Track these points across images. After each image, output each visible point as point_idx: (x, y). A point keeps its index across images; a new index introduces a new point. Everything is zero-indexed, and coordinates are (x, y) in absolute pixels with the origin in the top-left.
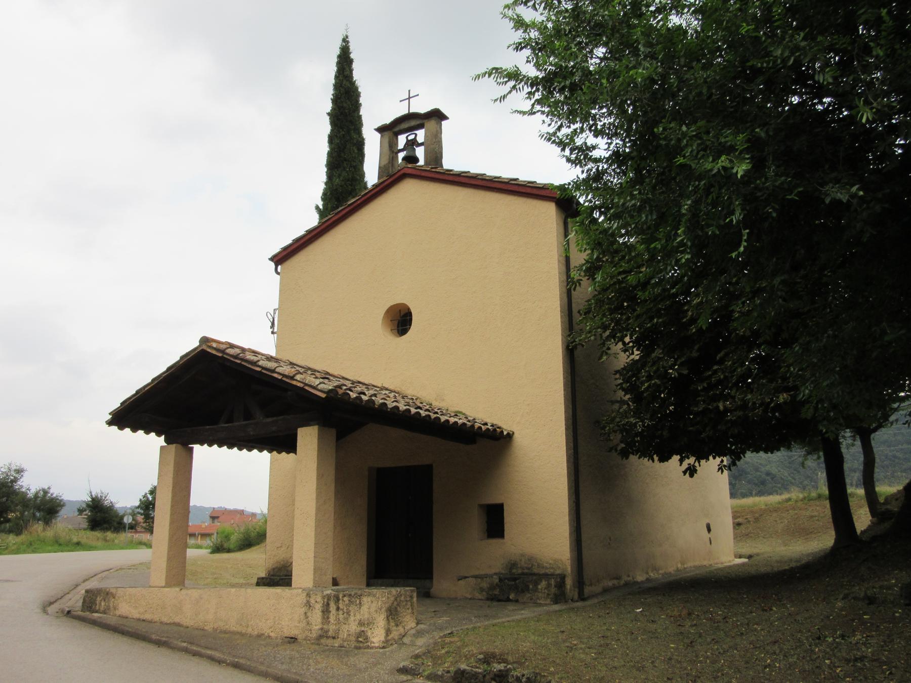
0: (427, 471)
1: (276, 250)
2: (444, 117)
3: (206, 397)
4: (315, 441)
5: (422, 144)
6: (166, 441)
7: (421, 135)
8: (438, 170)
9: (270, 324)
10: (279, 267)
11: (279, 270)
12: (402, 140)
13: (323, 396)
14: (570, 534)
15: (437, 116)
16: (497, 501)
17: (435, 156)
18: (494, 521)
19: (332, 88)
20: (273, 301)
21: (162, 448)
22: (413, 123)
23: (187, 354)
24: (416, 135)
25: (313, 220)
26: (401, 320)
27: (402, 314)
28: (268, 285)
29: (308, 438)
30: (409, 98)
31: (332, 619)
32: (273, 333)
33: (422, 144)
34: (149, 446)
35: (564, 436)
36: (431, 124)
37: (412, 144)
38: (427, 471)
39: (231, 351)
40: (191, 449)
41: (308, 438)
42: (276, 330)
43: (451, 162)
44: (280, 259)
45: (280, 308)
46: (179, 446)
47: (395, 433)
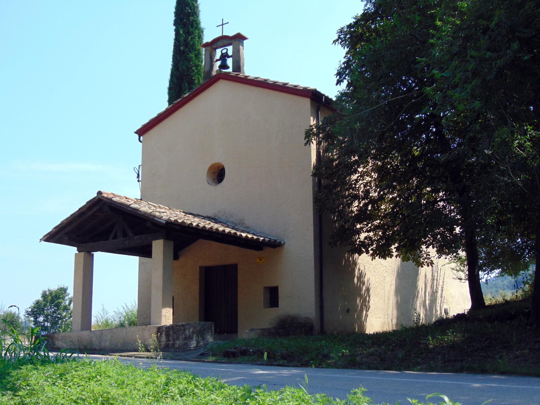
0: (234, 268)
1: (139, 127)
2: (245, 38)
3: (99, 226)
4: (162, 248)
5: (231, 56)
6: (78, 250)
7: (230, 50)
8: (241, 75)
9: (137, 175)
10: (141, 138)
11: (141, 139)
12: (218, 53)
13: (164, 222)
14: (316, 303)
15: (239, 38)
16: (275, 285)
17: (238, 67)
18: (273, 296)
19: (173, 15)
20: (138, 161)
21: (76, 254)
22: (225, 42)
23: (90, 201)
24: (227, 50)
25: (163, 105)
26: (218, 174)
27: (220, 169)
28: (135, 149)
29: (158, 246)
30: (223, 25)
31: (171, 338)
32: (138, 181)
33: (231, 56)
34: (69, 253)
35: (313, 245)
36: (236, 43)
37: (224, 57)
38: (234, 268)
39: (115, 199)
40: (93, 254)
41: (158, 246)
42: (140, 179)
43: (250, 70)
44: (142, 132)
45: (142, 165)
46: (86, 253)
47: (215, 245)
